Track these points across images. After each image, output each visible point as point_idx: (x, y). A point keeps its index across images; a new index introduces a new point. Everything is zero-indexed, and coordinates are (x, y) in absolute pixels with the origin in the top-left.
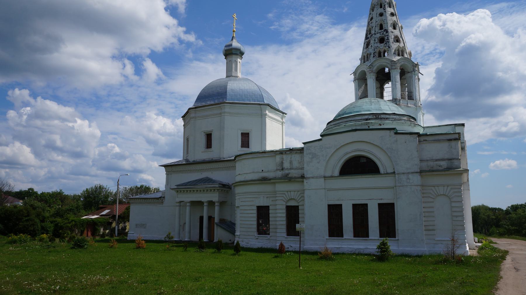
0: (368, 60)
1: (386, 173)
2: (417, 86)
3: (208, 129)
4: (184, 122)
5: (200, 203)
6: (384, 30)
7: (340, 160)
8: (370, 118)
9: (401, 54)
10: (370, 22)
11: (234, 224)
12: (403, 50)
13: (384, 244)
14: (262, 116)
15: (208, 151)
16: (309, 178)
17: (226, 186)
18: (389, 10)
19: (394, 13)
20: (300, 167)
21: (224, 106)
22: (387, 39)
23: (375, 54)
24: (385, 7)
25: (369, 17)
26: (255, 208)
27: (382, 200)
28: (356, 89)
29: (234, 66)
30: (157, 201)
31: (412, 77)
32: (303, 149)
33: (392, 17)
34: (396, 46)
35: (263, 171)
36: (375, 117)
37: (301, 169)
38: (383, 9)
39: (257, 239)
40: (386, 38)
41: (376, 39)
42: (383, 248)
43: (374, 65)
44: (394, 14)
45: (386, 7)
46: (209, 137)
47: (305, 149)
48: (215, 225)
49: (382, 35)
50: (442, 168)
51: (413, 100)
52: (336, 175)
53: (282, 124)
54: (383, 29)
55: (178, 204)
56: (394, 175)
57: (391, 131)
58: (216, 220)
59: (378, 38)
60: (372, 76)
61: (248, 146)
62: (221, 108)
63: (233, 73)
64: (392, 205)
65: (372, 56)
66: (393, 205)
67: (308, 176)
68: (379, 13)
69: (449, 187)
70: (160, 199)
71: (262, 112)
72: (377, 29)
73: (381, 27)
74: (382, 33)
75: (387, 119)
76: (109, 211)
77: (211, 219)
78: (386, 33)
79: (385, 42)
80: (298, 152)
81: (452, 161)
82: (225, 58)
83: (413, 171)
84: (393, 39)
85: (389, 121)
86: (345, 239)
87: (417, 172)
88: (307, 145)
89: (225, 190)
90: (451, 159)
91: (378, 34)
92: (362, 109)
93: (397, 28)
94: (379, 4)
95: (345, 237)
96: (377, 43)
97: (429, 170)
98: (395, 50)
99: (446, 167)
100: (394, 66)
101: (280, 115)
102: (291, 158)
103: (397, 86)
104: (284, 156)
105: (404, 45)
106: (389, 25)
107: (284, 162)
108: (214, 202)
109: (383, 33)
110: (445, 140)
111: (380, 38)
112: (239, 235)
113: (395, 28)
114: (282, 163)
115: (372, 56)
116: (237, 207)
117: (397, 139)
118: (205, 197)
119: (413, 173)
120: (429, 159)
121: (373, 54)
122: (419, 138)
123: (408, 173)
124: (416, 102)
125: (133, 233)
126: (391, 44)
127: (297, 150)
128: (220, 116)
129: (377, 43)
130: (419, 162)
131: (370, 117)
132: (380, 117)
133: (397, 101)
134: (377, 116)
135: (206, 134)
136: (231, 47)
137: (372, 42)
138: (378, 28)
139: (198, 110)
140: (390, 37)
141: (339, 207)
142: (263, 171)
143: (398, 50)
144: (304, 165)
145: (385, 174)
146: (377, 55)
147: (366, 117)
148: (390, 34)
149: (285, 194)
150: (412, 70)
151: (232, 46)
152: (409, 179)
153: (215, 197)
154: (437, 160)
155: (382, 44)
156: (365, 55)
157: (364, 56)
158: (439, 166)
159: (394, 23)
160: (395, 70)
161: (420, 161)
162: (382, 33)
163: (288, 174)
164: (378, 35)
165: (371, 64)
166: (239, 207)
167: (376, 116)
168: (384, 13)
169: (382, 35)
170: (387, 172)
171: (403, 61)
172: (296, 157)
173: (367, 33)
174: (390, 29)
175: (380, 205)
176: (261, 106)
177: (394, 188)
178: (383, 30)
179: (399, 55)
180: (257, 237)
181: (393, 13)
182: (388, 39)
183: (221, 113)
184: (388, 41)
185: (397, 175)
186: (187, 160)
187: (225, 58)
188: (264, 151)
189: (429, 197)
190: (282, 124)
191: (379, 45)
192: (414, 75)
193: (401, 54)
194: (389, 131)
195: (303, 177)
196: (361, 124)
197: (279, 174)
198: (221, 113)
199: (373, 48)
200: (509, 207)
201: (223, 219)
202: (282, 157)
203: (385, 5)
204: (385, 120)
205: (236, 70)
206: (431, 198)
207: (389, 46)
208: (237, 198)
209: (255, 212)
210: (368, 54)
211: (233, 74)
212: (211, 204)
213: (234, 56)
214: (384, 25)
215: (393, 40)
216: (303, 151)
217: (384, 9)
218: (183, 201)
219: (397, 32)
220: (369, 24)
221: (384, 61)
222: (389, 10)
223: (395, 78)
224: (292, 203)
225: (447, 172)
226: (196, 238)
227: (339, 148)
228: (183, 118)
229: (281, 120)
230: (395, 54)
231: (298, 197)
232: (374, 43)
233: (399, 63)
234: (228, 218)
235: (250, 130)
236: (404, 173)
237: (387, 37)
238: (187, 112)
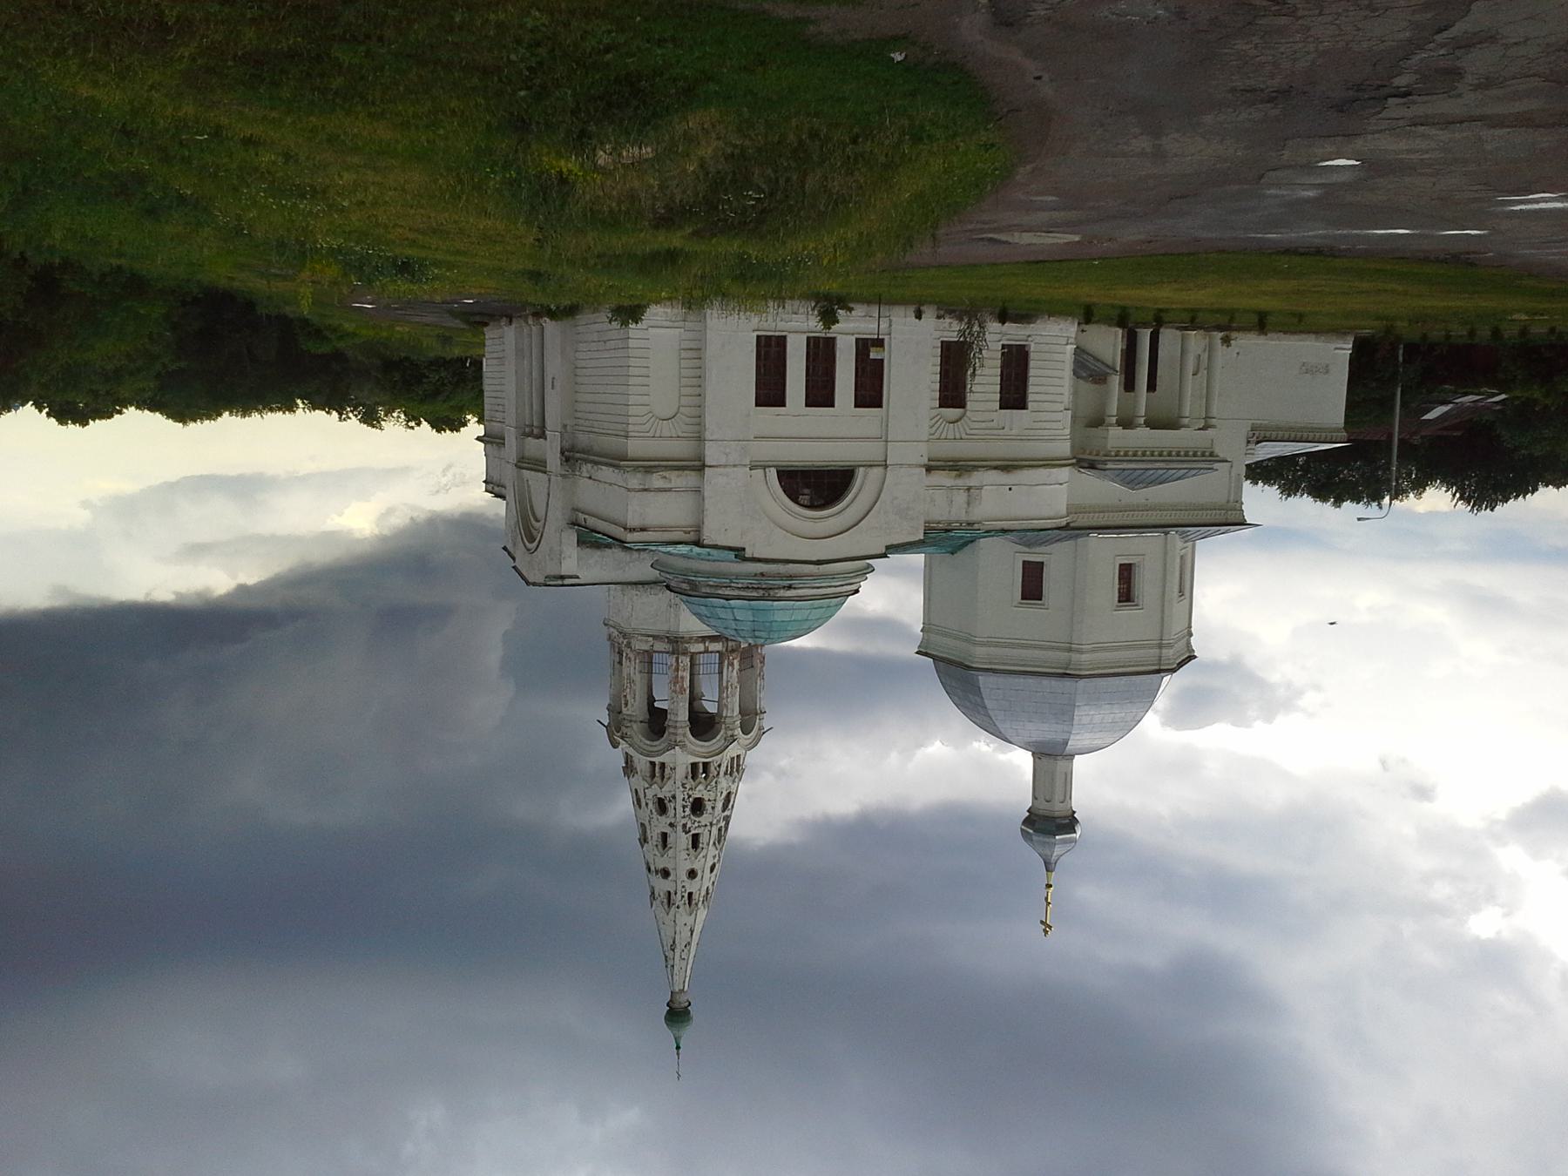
0: (732, 759)
3: (1127, 612)
4: (1189, 644)
5: (1153, 424)
6: (690, 831)
8: (782, 591)
13: (827, 326)
16: (921, 466)
17: (1086, 465)
22: (687, 806)
26: (1030, 405)
30: (1268, 434)
35: (1010, 489)
36: (772, 593)
39: (1029, 336)
41: (710, 810)
42: (829, 318)
46: (1126, 595)
48: (1118, 369)
50: (661, 473)
52: (861, 469)
55: (1214, 421)
58: (1116, 381)
61: (1027, 565)
65: (723, 769)
67: (918, 470)
68: (697, 879)
70: (1261, 438)
72: (703, 839)
74: (696, 824)
75: (748, 588)
76: (1425, 418)
77: (1129, 385)
80: (935, 525)
82: (1074, 812)
85: (742, 583)
86: (853, 334)
87: (710, 466)
89: (1090, 454)
90: (645, 490)
95: (853, 339)
96: (709, 800)
99: (654, 475)
102: (950, 512)
107: (966, 506)
108: (1119, 426)
112: (1067, 344)
115: (723, 769)
116: (1068, 410)
118: (1142, 437)
121: (722, 773)
123: (725, 466)
125: (1337, 351)
129: (709, 800)
135: (1133, 602)
137: (719, 805)
139: (1153, 665)
141: (860, 403)
142: (1010, 489)
149: (967, 434)
153: (1116, 437)
157: (738, 771)
159: (664, 849)
162: (696, 824)
163: (959, 476)
164: (705, 819)
166: (1066, 409)
169: (697, 819)
178: (693, 832)
179: (663, 765)
180: (1030, 339)
184: (684, 803)
186: (1183, 536)
187: (1074, 812)
189: (688, 417)
195: (929, 469)
197: (975, 479)
200: (120, 412)
201: (1096, 383)
204: (751, 584)
208: (1067, 431)
209: (1031, 397)
210: (731, 775)
211: (1168, 331)
212: (1126, 423)
218: (1200, 429)
224: (953, 413)
226: (1168, 337)
231: (937, 421)
234: (1087, 387)
236: (735, 466)
238: (1181, 665)
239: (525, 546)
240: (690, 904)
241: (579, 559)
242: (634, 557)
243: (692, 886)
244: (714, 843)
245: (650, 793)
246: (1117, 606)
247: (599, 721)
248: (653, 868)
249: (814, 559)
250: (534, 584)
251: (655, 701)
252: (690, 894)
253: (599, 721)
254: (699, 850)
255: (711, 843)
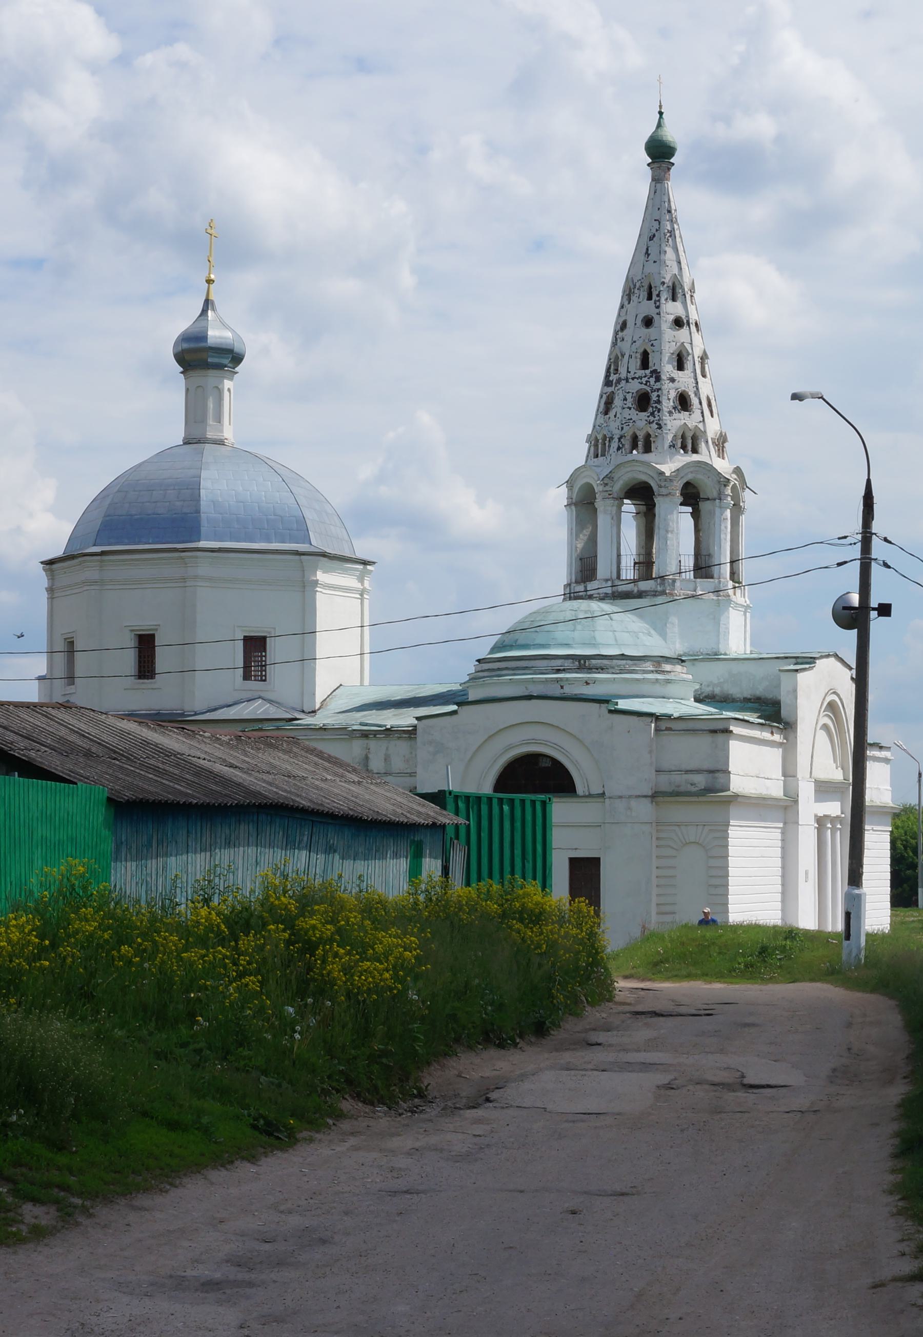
0: (603, 455)
1: (587, 794)
2: (725, 539)
3: (145, 624)
6: (651, 372)
7: (495, 761)
9: (689, 447)
10: (620, 334)
11: (849, 884)
12: (697, 434)
14: (304, 587)
15: (143, 686)
18: (672, 309)
19: (683, 317)
20: (409, 771)
21: (196, 557)
23: (622, 440)
24: (659, 301)
25: (619, 315)
27: (577, 850)
28: (572, 529)
29: (211, 405)
31: (714, 513)
32: (416, 730)
33: (678, 330)
34: (679, 423)
37: (411, 776)
38: (655, 303)
40: (654, 397)
41: (629, 396)
43: (616, 476)
44: (683, 322)
45: (663, 301)
47: (419, 731)
49: (645, 387)
50: (697, 789)
51: (712, 577)
53: (362, 595)
54: (648, 369)
56: (602, 800)
57: (602, 705)
59: (635, 395)
60: (610, 508)
62: (186, 564)
63: (208, 429)
64: (595, 862)
65: (615, 444)
66: (598, 860)
69: (706, 827)
71: (303, 576)
72: (636, 362)
73: (645, 364)
74: (644, 380)
78: (655, 382)
79: (650, 410)
81: (717, 775)
83: (638, 794)
84: (671, 401)
85: (608, 673)
88: (424, 721)
91: (636, 380)
92: (553, 639)
93: (688, 365)
94: (646, 287)
96: (630, 408)
97: (671, 791)
98: (675, 436)
99: (703, 788)
100: (665, 487)
101: (356, 570)
103: (668, 542)
104: (372, 744)
105: (701, 419)
106: (666, 357)
107: (370, 756)
109: (647, 381)
110: (705, 732)
111: (640, 394)
113: (680, 366)
114: (367, 758)
115: (615, 444)
117: (612, 724)
119: (638, 797)
120: (673, 768)
121: (616, 440)
122: (658, 723)
123: (630, 797)
124: (720, 582)
126: (666, 418)
127: (402, 732)
128: (182, 585)
130: (655, 773)
131: (568, 664)
132: (589, 665)
133: (666, 585)
134: (582, 662)
136: (202, 345)
137: (618, 402)
138: (637, 362)
140: (664, 397)
143: (683, 437)
144: (416, 767)
145: (585, 796)
146: (627, 443)
147: (559, 662)
148: (666, 385)
150: (715, 494)
151: (206, 341)
152: (629, 808)
154: (687, 772)
155: (643, 415)
156: (600, 437)
157: (597, 440)
158: (692, 785)
159: (681, 351)
160: (667, 499)
161: (656, 771)
164: (635, 387)
165: (607, 475)
167: (579, 662)
168: (656, 317)
169: (643, 387)
170: (589, 792)
171: (692, 472)
172: (399, 748)
173: (610, 365)
174: (668, 369)
175: (572, 860)
176: (303, 557)
177: (600, 826)
178: (648, 372)
181: (680, 317)
182: (659, 402)
183: (184, 579)
184: (659, 407)
185: (607, 800)
188: (324, 726)
189: (669, 846)
190: (362, 595)
191: (634, 414)
192: (720, 507)
193: (689, 447)
194: (597, 705)
196: (544, 680)
198: (184, 579)
199: (618, 423)
202: (367, 744)
203: (659, 292)
204: (599, 673)
205: (219, 419)
206: (672, 848)
207: (661, 422)
210: (605, 437)
213: (211, 373)
214: (653, 357)
215: (672, 404)
216: (416, 734)
217: (658, 304)
219: (684, 380)
220: (616, 340)
221: (641, 469)
222: (672, 309)
223: (665, 520)
225: (701, 799)
227: (493, 735)
228: (48, 567)
229: (359, 586)
230: (674, 447)
232: (624, 408)
233: (678, 479)
235: (269, 630)
236: (620, 797)
237: (655, 394)
239: (838, 695)
240: (650, 287)
241: (778, 686)
242: (719, 688)
243: (647, 308)
244: (623, 356)
245: (697, 415)
246: (156, 630)
247: (755, 493)
248: (693, 328)
249: (534, 701)
250: (828, 656)
251: (691, 513)
252: (650, 298)
253: (755, 493)
254: (642, 350)
255: (626, 357)
